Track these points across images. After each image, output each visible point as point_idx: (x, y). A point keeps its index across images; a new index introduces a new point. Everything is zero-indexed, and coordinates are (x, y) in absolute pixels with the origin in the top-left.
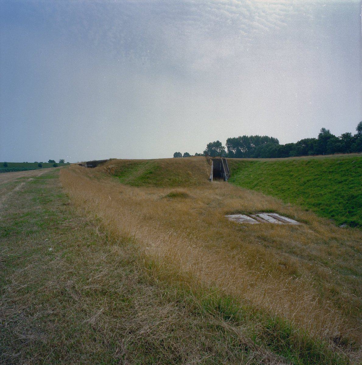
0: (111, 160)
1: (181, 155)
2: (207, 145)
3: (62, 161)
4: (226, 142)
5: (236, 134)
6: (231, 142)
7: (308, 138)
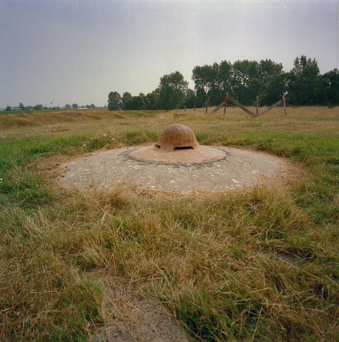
0: (38, 108)
1: (119, 96)
2: (161, 79)
3: (21, 106)
4: (191, 74)
5: (210, 59)
6: (201, 74)
7: (131, 94)
